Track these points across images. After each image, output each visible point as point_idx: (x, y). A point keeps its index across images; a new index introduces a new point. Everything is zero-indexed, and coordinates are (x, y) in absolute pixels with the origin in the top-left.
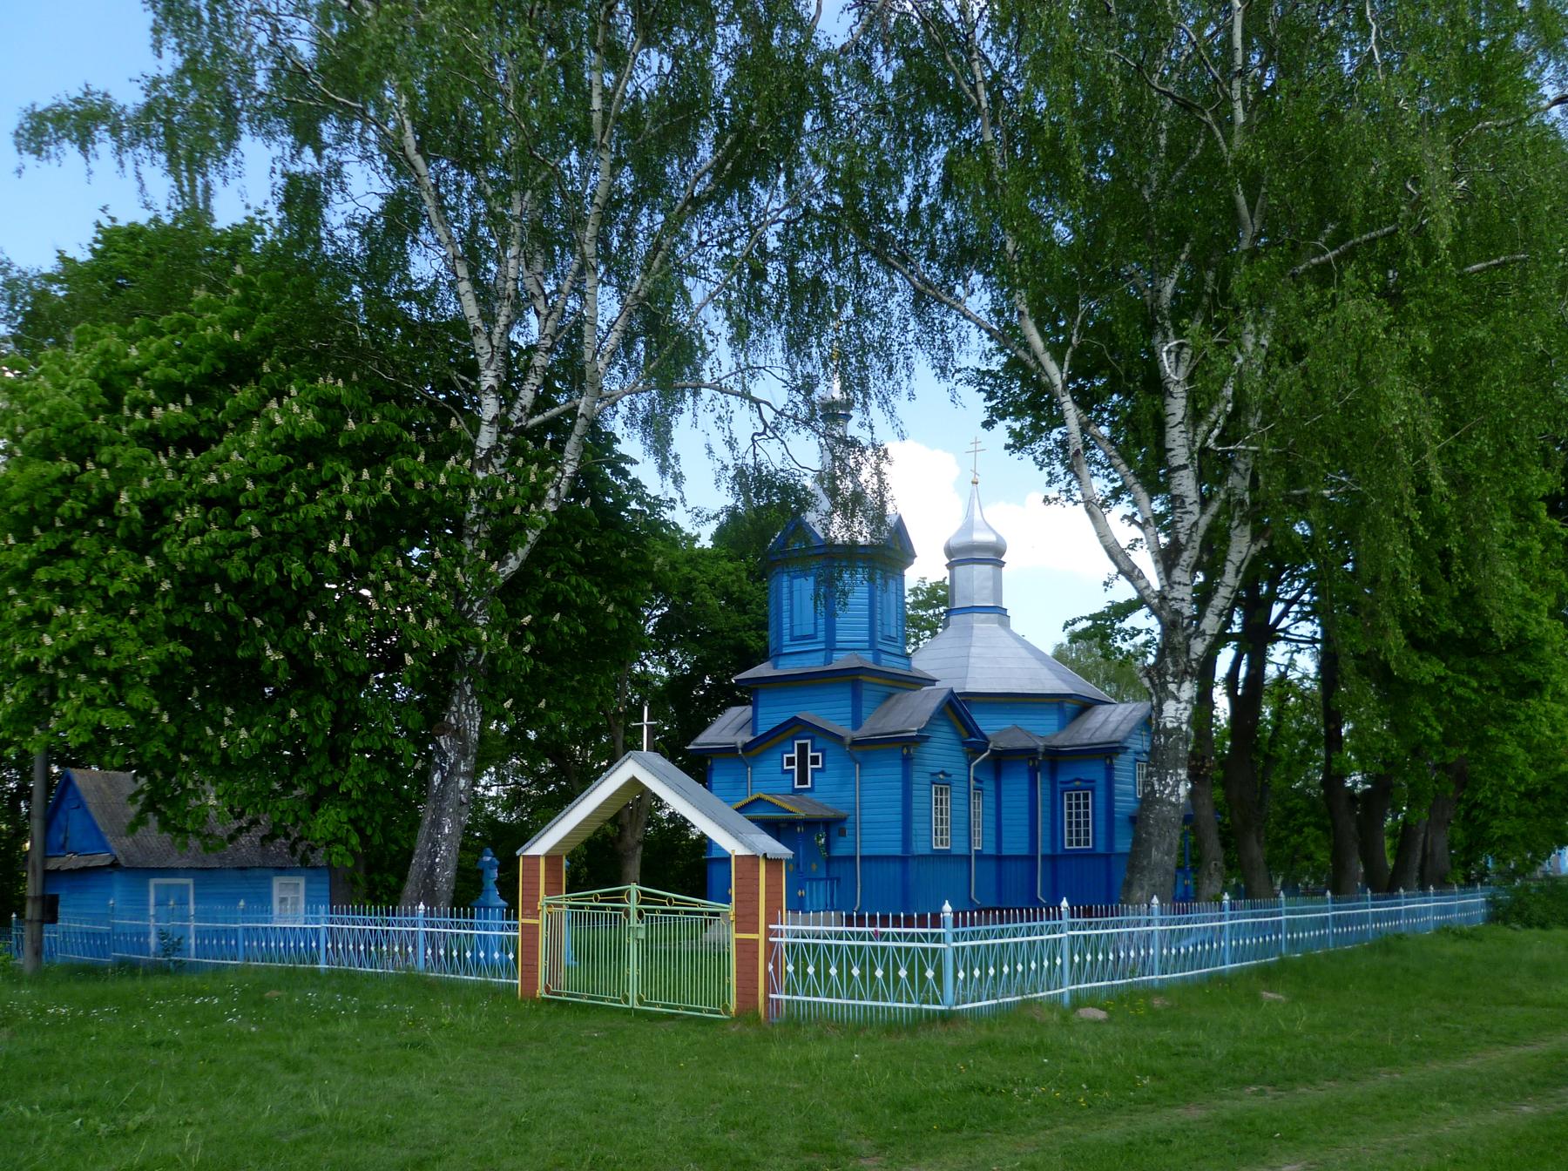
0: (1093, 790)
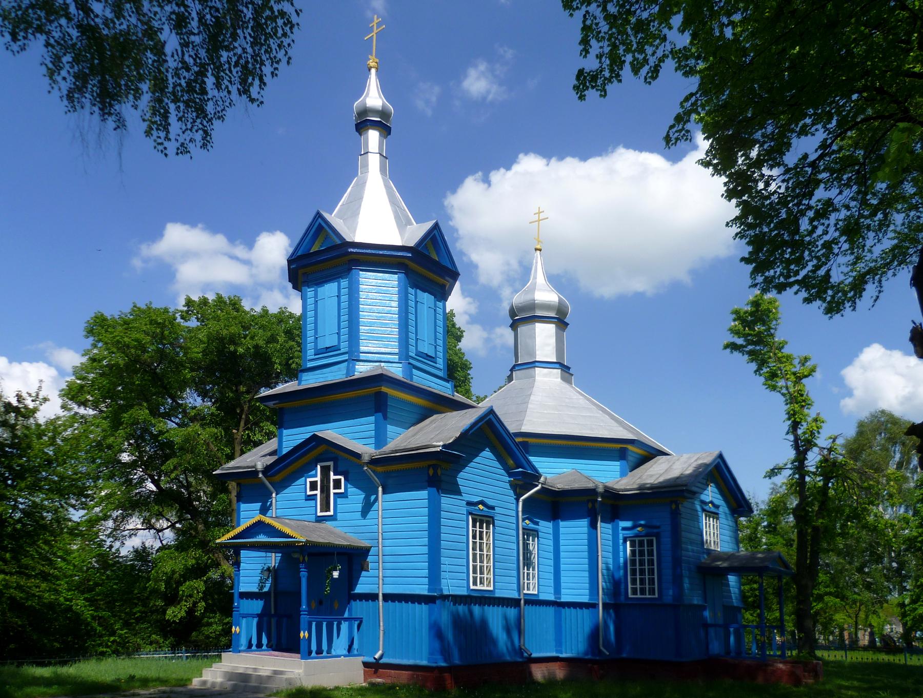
0: (658, 536)
